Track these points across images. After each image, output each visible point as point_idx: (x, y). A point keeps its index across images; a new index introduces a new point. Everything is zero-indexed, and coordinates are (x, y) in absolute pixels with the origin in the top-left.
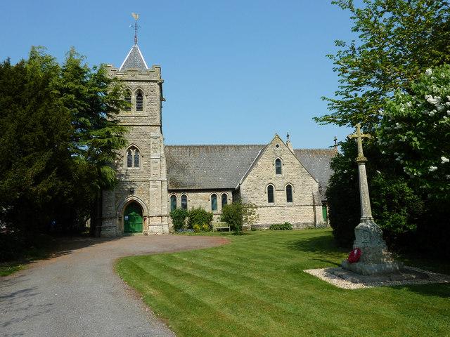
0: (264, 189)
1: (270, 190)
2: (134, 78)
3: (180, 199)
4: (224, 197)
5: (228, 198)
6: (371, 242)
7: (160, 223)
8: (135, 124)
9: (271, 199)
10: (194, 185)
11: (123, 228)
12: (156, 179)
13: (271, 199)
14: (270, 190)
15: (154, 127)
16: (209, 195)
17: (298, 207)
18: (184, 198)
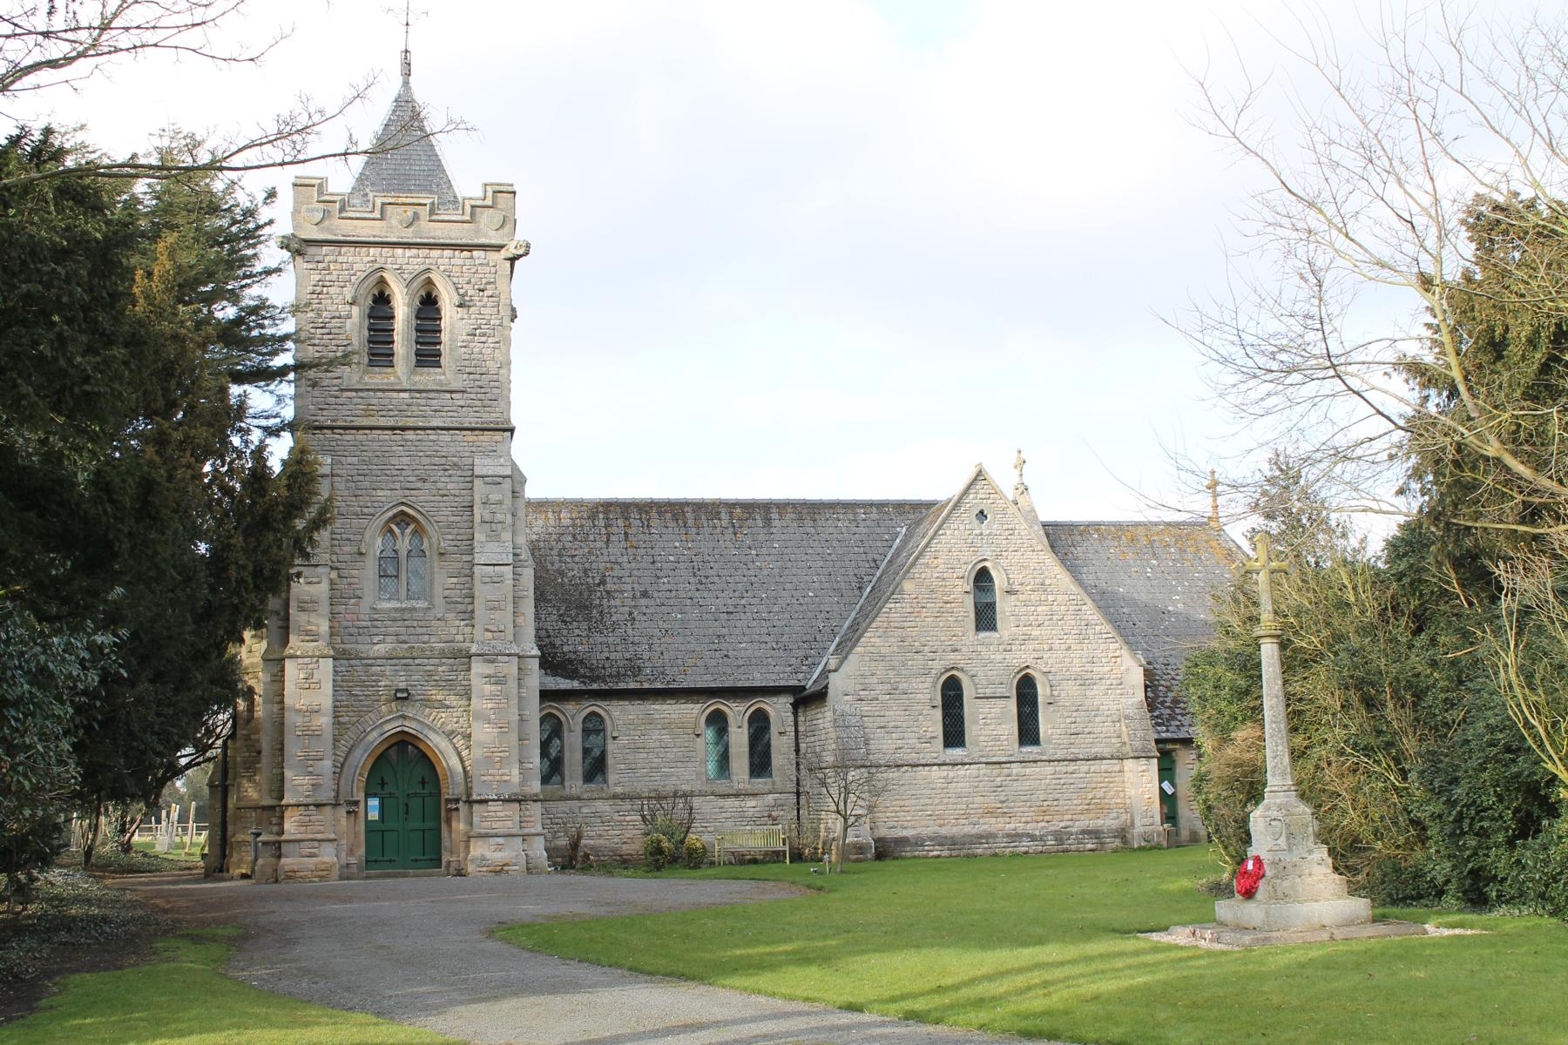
0: (928, 693)
1: (952, 695)
2: (409, 235)
3: (578, 729)
4: (759, 723)
5: (774, 730)
6: (1290, 850)
7: (511, 826)
8: (411, 422)
9: (954, 734)
10: (636, 671)
11: (362, 851)
12: (500, 647)
13: (954, 734)
14: (952, 695)
15: (487, 436)
16: (695, 712)
17: (1062, 767)
18: (594, 726)
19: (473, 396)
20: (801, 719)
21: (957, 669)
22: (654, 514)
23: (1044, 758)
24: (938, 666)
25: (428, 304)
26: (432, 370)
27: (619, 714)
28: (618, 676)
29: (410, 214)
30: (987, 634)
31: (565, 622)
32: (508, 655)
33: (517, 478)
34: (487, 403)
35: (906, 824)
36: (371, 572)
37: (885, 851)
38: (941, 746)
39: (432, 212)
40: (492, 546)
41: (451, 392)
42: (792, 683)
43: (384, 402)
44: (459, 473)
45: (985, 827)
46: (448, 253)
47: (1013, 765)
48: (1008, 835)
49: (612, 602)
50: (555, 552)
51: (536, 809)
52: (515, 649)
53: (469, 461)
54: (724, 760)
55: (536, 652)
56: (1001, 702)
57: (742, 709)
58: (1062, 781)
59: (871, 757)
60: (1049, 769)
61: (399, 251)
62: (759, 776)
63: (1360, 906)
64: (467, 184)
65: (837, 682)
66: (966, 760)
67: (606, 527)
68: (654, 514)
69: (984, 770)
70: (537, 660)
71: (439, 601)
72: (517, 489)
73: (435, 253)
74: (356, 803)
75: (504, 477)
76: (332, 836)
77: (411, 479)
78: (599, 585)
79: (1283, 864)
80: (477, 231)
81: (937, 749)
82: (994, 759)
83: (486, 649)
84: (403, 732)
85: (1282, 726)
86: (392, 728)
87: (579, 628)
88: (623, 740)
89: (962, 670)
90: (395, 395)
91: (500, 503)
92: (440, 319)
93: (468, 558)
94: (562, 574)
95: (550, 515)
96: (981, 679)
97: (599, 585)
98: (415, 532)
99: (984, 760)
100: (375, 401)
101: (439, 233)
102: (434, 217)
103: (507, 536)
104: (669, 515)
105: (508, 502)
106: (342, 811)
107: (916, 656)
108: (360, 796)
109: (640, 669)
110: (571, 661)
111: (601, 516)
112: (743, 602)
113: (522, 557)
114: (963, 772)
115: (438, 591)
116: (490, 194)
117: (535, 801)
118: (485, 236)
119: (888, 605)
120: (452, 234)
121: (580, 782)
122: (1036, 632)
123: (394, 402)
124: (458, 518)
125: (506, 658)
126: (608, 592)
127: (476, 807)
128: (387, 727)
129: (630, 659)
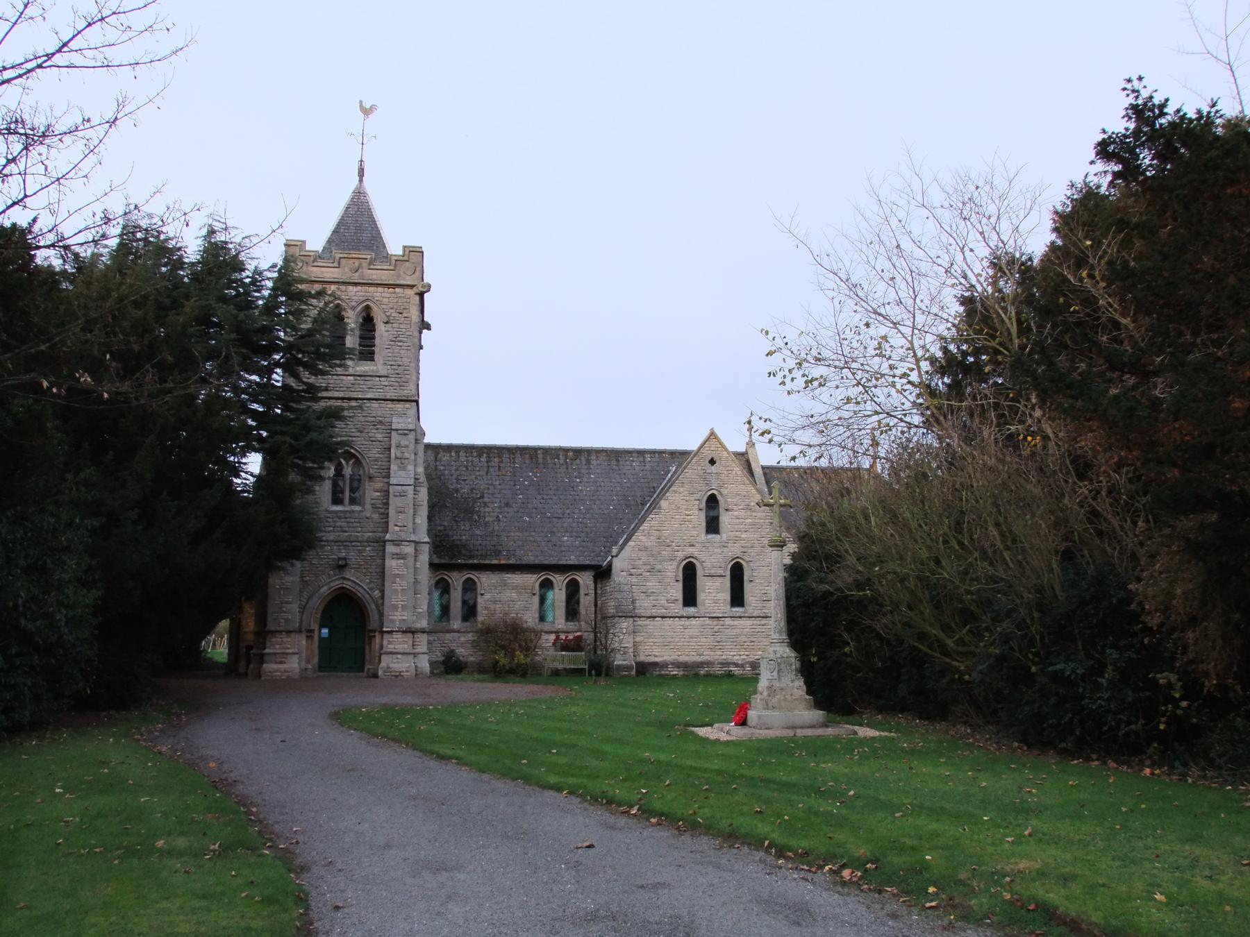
0: (673, 572)
1: (689, 574)
2: (356, 278)
3: (460, 589)
4: (573, 590)
5: (582, 592)
7: (406, 647)
8: (355, 395)
9: (690, 598)
10: (497, 553)
12: (404, 536)
13: (690, 598)
14: (689, 574)
17: (757, 622)
18: (470, 586)
19: (393, 379)
20: (599, 586)
21: (693, 557)
22: (518, 455)
23: (746, 615)
24: (680, 555)
25: (368, 322)
26: (369, 362)
27: (486, 581)
28: (485, 556)
29: (357, 264)
30: (714, 536)
31: (456, 521)
32: (409, 541)
33: (419, 431)
34: (401, 384)
35: (657, 654)
36: (327, 488)
37: (643, 669)
38: (681, 606)
39: (370, 264)
40: (402, 473)
41: (380, 377)
42: (593, 563)
43: (338, 382)
44: (383, 427)
45: (707, 657)
46: (380, 289)
47: (726, 619)
48: (721, 664)
49: (487, 510)
50: (454, 477)
51: (423, 639)
52: (413, 538)
53: (389, 420)
54: (445, 610)
55: (427, 539)
56: (720, 580)
57: (563, 578)
58: (757, 630)
59: (636, 611)
60: (749, 622)
61: (350, 288)
62: (570, 621)
63: (818, 715)
64: (394, 247)
65: (618, 564)
66: (697, 615)
67: (487, 462)
68: (518, 455)
69: (707, 621)
70: (428, 545)
71: (368, 506)
72: (419, 437)
73: (372, 289)
74: (312, 631)
75: (411, 430)
76: (296, 650)
77: (353, 430)
78: (479, 498)
79: (774, 688)
80: (399, 276)
81: (678, 608)
82: (714, 615)
83: (395, 537)
84: (343, 588)
85: (781, 602)
86: (335, 584)
87: (465, 526)
88: (487, 596)
89: (696, 558)
90: (344, 378)
91: (407, 447)
92: (375, 331)
93: (386, 480)
94: (457, 491)
95: (453, 454)
96: (706, 564)
97: (479, 498)
98: (354, 464)
99: (708, 615)
100: (332, 381)
101: (374, 277)
102: (372, 267)
103: (411, 467)
104: (527, 456)
105: (412, 446)
106: (304, 636)
107: (668, 549)
108: (315, 627)
109: (500, 552)
110: (457, 546)
111: (485, 455)
112: (568, 511)
113: (420, 481)
114: (694, 622)
115: (368, 501)
116: (407, 252)
117: (423, 632)
118: (404, 279)
119: (651, 516)
120: (383, 278)
121: (460, 622)
122: (744, 536)
123: (344, 382)
124: (381, 456)
125: (407, 543)
126: (485, 503)
127: (386, 636)
128: (332, 584)
129: (495, 546)
